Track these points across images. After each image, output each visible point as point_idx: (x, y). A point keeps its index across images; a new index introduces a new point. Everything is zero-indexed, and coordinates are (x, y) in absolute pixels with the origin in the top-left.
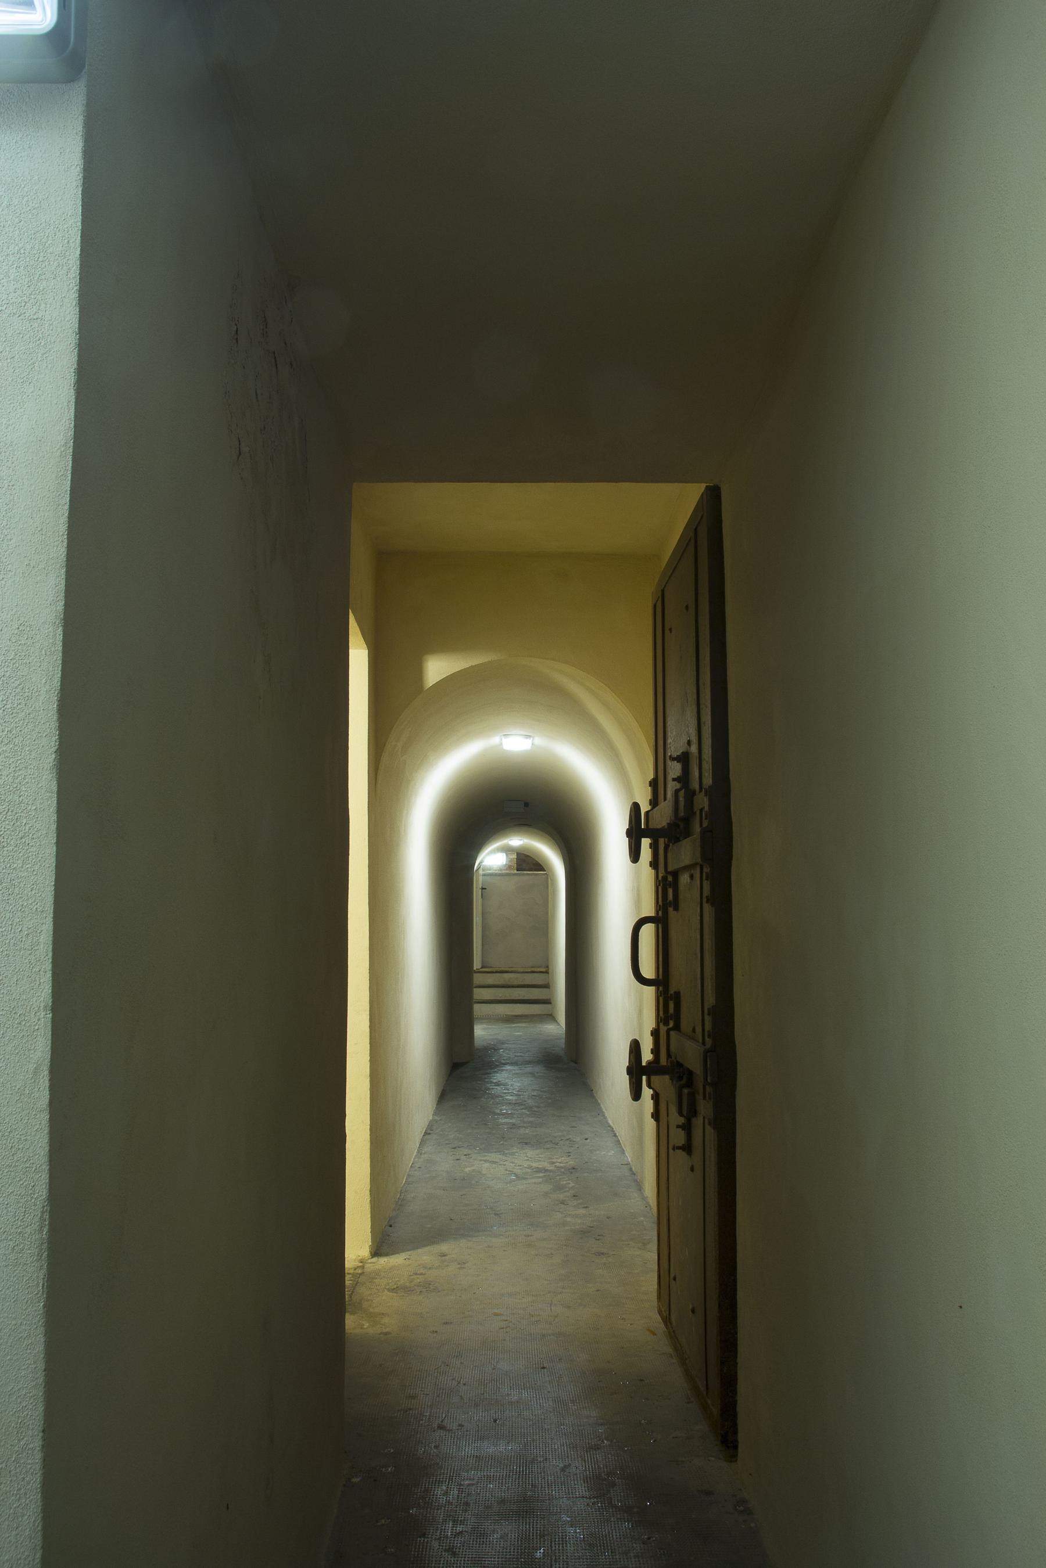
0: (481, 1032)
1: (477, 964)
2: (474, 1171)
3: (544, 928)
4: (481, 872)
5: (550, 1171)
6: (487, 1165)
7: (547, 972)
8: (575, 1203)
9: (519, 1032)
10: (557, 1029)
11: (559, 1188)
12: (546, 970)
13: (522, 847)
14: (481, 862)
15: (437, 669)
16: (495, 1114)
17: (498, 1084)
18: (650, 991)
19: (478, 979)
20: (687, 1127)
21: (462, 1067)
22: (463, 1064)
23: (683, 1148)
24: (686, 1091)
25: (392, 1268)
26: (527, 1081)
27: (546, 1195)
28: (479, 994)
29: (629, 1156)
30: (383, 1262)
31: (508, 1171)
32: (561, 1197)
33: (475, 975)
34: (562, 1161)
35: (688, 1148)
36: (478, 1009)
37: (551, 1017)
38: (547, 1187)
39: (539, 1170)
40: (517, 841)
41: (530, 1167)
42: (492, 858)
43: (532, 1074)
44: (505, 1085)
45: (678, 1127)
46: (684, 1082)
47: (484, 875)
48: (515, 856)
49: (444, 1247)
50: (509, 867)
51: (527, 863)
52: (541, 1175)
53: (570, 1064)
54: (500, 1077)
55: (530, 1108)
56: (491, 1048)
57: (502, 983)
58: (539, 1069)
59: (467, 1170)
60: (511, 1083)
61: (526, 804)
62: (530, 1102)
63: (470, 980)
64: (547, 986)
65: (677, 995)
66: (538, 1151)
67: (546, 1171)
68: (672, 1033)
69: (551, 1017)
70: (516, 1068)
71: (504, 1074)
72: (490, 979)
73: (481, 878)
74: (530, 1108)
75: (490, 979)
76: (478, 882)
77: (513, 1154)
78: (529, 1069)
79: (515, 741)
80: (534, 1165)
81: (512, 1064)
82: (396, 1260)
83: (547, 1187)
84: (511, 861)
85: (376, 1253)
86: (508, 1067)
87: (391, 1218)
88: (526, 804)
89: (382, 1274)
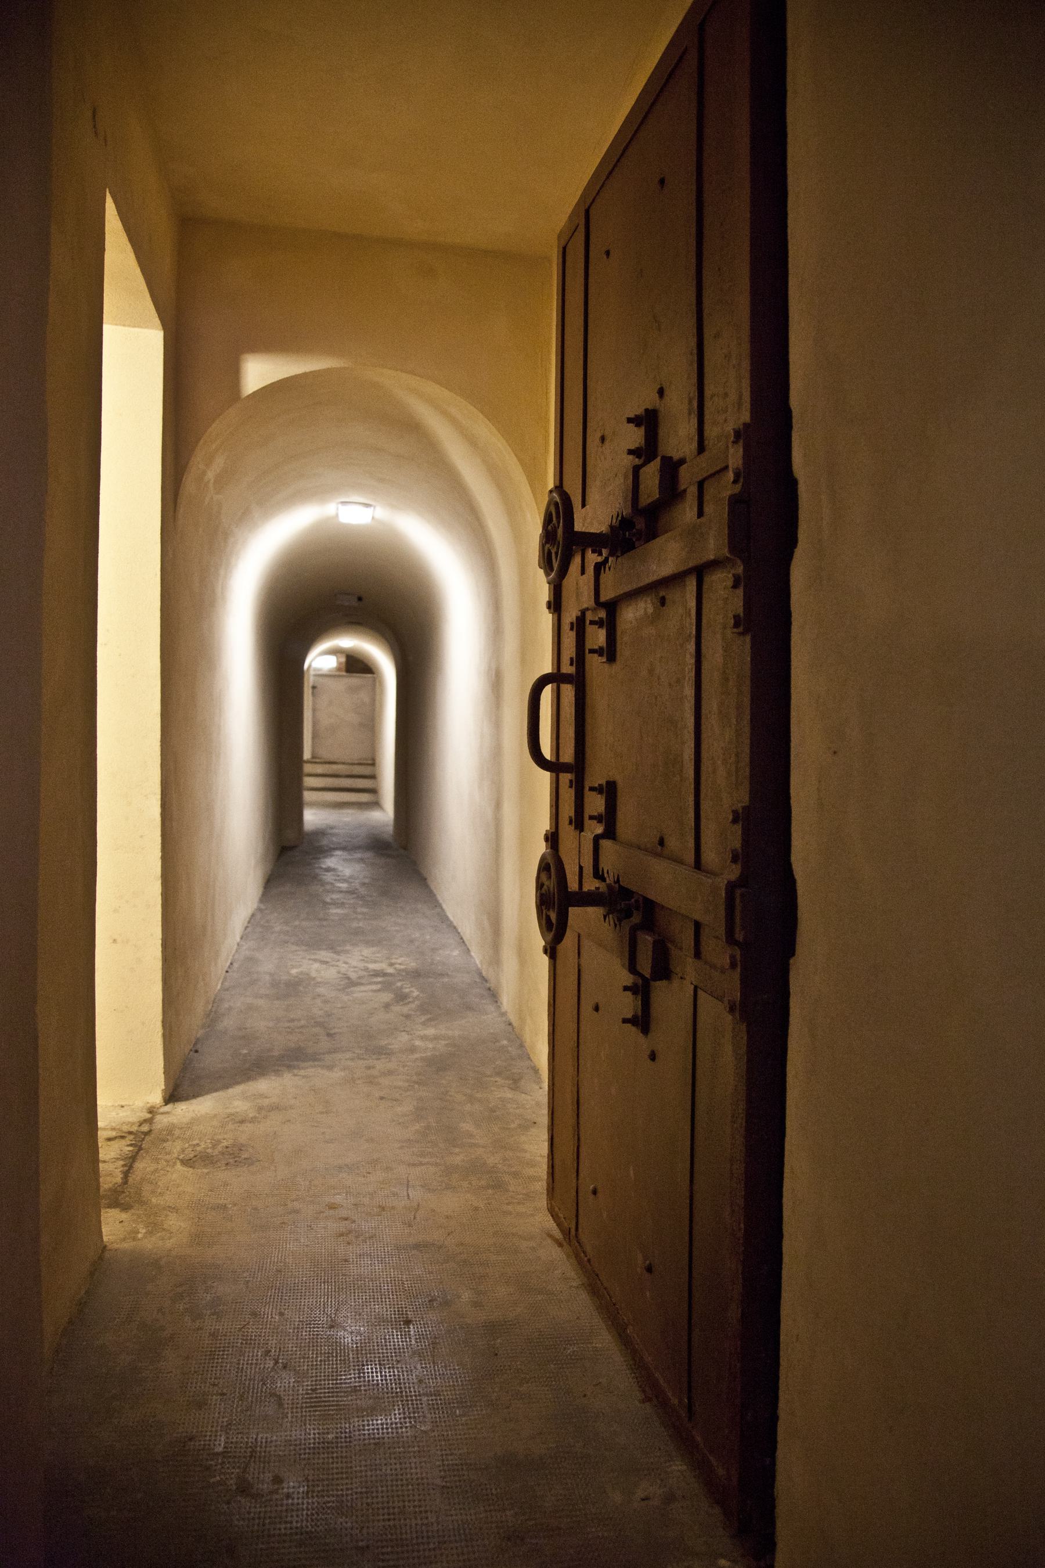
0: (312, 818)
1: (307, 755)
2: (301, 973)
3: (371, 725)
4: (312, 673)
5: (391, 975)
6: (316, 965)
7: (373, 764)
8: (423, 1018)
9: (348, 818)
10: (385, 814)
11: (401, 998)
12: (372, 762)
13: (350, 649)
14: (310, 666)
15: (258, 373)
16: (325, 903)
17: (328, 870)
18: (544, 778)
19: (308, 768)
20: (641, 990)
21: (290, 852)
22: (292, 848)
23: (633, 1021)
24: (646, 940)
25: (194, 1121)
26: (358, 867)
27: (387, 1006)
28: (309, 782)
29: (477, 957)
30: (183, 1111)
31: (343, 969)
32: (405, 1010)
33: (562, 760)
34: (405, 962)
35: (642, 1021)
36: (308, 796)
37: (376, 804)
38: (387, 997)
39: (377, 974)
40: (349, 641)
41: (366, 969)
42: (321, 659)
43: (362, 860)
44: (334, 870)
45: (626, 988)
46: (636, 919)
47: (315, 675)
48: (343, 660)
49: (263, 1085)
50: (339, 669)
51: (356, 665)
52: (380, 979)
53: (404, 852)
54: (330, 862)
55: (362, 897)
56: (320, 833)
57: (330, 772)
58: (368, 855)
59: (294, 971)
60: (342, 869)
61: (360, 599)
62: (363, 891)
63: (300, 768)
64: (373, 777)
65: (610, 791)
66: (374, 949)
67: (385, 975)
68: (605, 844)
69: (376, 804)
70: (345, 853)
71: (333, 859)
72: (319, 769)
73: (312, 679)
74: (362, 897)
75: (319, 769)
76: (309, 681)
77: (347, 952)
78: (358, 855)
79: (354, 511)
80: (372, 966)
81: (344, 849)
82: (201, 1107)
83: (387, 997)
84: (339, 663)
85: (172, 1096)
86: (338, 853)
87: (198, 1041)
88: (360, 599)
89: (177, 1132)
